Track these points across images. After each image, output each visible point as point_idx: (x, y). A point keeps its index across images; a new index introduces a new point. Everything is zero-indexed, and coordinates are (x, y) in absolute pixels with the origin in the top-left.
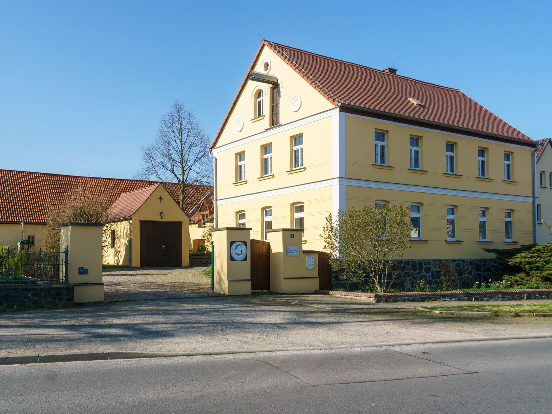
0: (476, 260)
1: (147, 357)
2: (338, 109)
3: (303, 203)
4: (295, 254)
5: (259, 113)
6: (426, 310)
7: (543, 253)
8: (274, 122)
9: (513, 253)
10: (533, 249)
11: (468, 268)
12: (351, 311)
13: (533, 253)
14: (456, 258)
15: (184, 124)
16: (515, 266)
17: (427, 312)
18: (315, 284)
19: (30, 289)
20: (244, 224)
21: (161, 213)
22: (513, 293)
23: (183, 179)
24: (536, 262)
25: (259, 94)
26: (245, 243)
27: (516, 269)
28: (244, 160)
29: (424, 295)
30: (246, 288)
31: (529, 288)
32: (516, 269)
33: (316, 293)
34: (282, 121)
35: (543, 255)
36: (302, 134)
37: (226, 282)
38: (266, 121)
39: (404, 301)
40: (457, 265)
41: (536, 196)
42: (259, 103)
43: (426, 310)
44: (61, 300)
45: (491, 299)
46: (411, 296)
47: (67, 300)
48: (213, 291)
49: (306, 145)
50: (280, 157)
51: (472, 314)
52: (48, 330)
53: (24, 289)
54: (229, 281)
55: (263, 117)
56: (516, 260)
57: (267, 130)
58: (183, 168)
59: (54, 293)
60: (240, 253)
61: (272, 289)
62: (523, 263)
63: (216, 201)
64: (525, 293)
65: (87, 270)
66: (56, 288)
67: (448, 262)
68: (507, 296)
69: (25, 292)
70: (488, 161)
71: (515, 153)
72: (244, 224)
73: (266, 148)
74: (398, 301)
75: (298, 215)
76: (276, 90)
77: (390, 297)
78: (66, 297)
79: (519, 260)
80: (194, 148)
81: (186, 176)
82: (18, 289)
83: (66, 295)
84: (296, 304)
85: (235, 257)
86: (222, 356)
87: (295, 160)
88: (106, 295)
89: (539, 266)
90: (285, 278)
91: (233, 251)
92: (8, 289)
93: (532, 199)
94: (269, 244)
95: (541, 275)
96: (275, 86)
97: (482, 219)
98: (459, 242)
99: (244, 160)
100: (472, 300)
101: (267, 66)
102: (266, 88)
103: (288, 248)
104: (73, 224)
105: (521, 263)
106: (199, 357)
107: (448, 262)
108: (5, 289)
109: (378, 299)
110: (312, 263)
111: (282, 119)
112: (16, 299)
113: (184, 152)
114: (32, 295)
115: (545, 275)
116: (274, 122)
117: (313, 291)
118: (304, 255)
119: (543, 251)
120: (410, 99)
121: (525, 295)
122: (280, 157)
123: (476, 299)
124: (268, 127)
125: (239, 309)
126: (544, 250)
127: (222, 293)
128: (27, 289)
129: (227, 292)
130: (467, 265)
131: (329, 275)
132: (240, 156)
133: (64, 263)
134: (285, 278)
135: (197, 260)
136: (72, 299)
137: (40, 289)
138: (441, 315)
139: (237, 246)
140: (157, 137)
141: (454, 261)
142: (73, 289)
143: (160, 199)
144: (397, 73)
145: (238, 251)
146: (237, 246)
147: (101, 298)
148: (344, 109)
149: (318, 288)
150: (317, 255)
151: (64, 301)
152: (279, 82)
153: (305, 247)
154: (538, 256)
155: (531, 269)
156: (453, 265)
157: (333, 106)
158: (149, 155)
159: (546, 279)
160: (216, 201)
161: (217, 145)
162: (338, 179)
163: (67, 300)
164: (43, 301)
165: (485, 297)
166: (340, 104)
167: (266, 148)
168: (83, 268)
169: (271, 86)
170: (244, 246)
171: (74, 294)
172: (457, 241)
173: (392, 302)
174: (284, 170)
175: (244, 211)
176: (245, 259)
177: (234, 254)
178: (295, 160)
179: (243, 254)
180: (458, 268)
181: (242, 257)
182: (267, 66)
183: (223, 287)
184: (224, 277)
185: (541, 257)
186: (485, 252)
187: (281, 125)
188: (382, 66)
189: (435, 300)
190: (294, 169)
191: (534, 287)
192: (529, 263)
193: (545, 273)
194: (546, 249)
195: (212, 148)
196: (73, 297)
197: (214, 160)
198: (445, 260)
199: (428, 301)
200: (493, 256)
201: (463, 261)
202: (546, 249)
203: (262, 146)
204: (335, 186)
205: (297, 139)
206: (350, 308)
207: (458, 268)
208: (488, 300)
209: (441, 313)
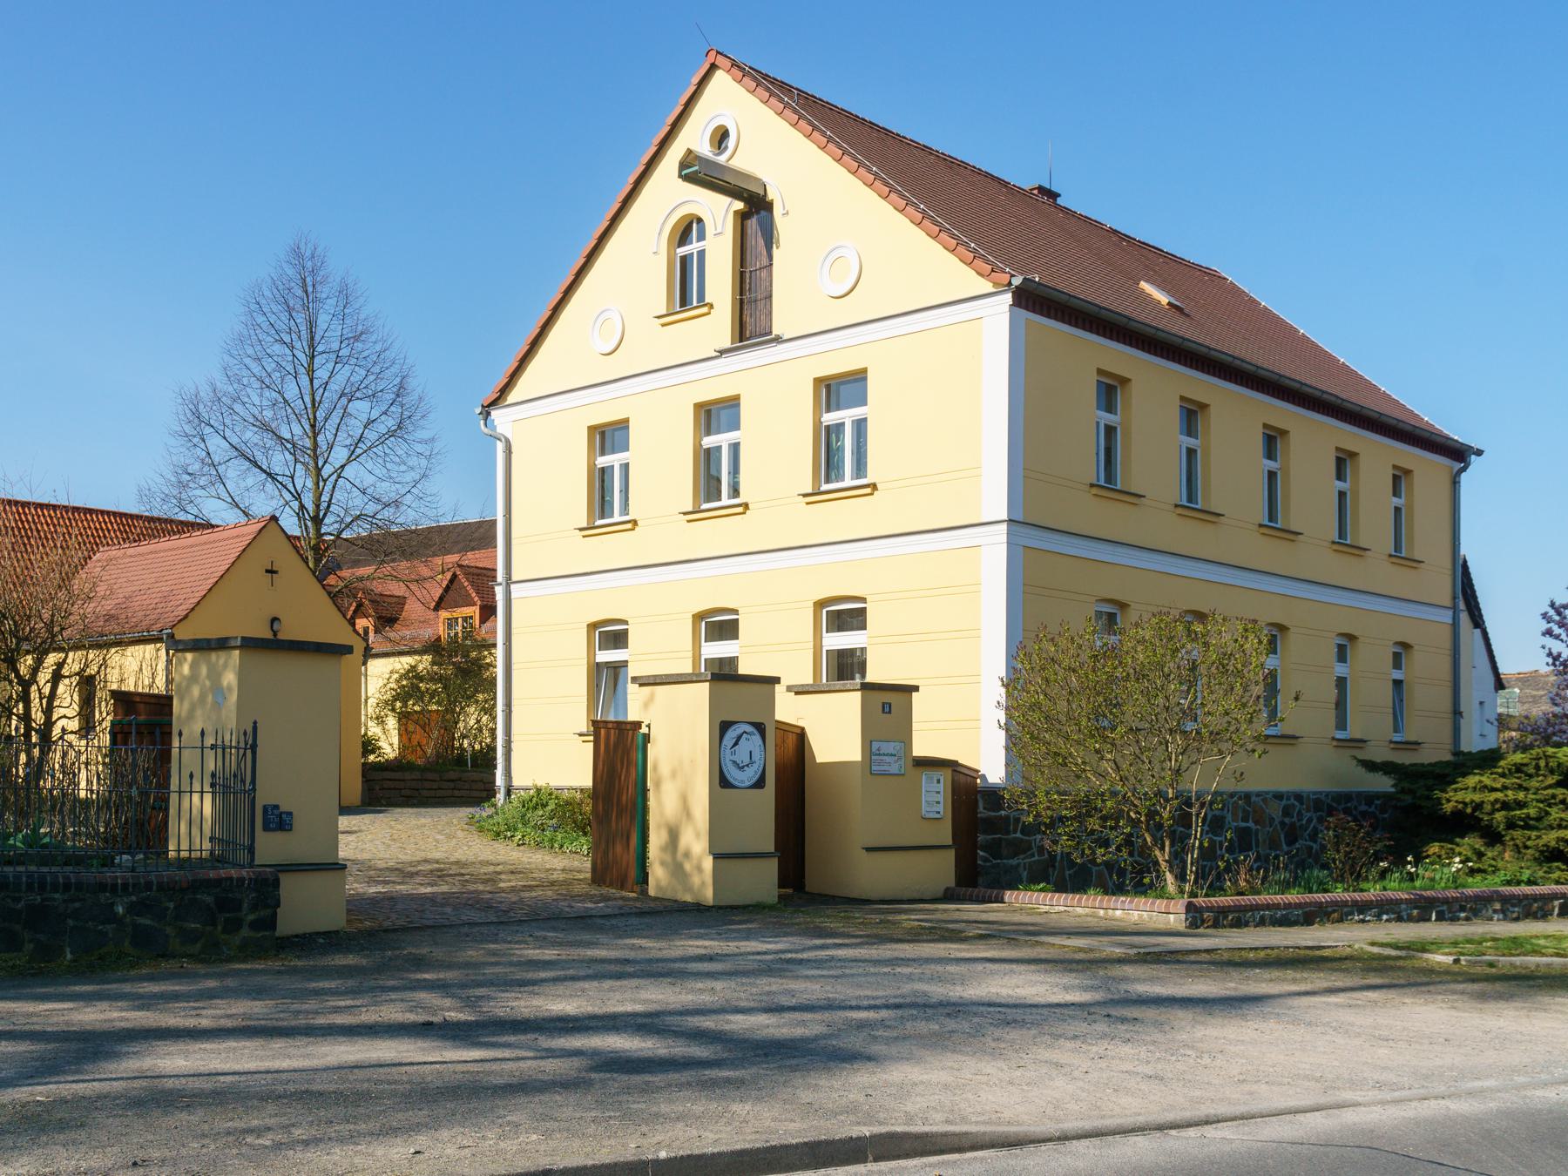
0: (1315, 793)
1: (982, 1147)
2: (1008, 298)
3: (863, 600)
4: (894, 769)
5: (685, 289)
6: (1394, 953)
7: (1531, 776)
8: (751, 324)
9: (1446, 775)
10: (1502, 763)
11: (1310, 820)
12: (1192, 957)
13: (1503, 775)
14: (1283, 788)
15: (323, 320)
16: (1458, 814)
17: (1399, 958)
18: (941, 868)
19: (125, 886)
20: (733, 661)
21: (274, 620)
22: (1526, 896)
23: (318, 506)
24: (1521, 805)
25: (688, 229)
26: (760, 728)
27: (1462, 823)
28: (626, 449)
29: (1310, 904)
30: (763, 880)
31: (1509, 883)
32: (1462, 823)
33: (949, 896)
34: (781, 324)
35: (1534, 783)
36: (864, 371)
37: (708, 863)
38: (718, 324)
39: (1262, 923)
40: (1287, 812)
41: (265, 633)
42: (685, 261)
43: (1394, 953)
44: (234, 926)
45: (1476, 915)
46: (1277, 906)
47: (254, 926)
48: (645, 892)
49: (878, 409)
50: (776, 443)
51: (1549, 965)
52: (204, 1043)
53: (102, 887)
54: (717, 857)
55: (705, 310)
56: (1460, 796)
57: (722, 352)
58: (319, 470)
59: (209, 899)
60: (747, 761)
61: (812, 883)
62: (1488, 807)
63: (508, 585)
64: (1555, 896)
65: (290, 814)
66: (218, 882)
67: (1265, 800)
68: (1514, 905)
69: (104, 897)
70: (1356, 493)
71: (1416, 474)
72: (733, 661)
73: (716, 414)
74: (1247, 925)
75: (839, 641)
76: (753, 223)
77: (1222, 912)
78: (251, 917)
79: (1469, 797)
80: (355, 406)
81: (325, 498)
82: (79, 886)
83: (254, 908)
84: (981, 937)
85: (733, 774)
86: (1210, 1131)
87: (835, 459)
88: (358, 906)
89: (1528, 816)
90: (868, 849)
91: (727, 757)
92: (42, 886)
93: (1450, 613)
94: (801, 735)
95: (1541, 842)
96: (756, 207)
97: (1341, 670)
98: (1290, 739)
99: (626, 449)
100: (1429, 920)
101: (720, 137)
102: (719, 211)
103: (875, 745)
104: (250, 644)
105: (1478, 806)
106: (1139, 1141)
107: (1265, 800)
108: (30, 887)
109: (1196, 917)
110: (935, 796)
111: (784, 316)
112: (71, 922)
113: (320, 414)
114: (131, 909)
115: (1553, 844)
116: (751, 324)
117: (940, 894)
118: (919, 769)
119: (1532, 771)
120: (1144, 285)
121: (1556, 903)
122: (776, 443)
123: (1506, 916)
124: (728, 344)
125: (840, 953)
126: (1537, 767)
127: (688, 898)
128: (114, 886)
129: (708, 896)
130: (1308, 810)
131: (991, 842)
132: (609, 436)
133: (207, 788)
134: (868, 849)
135: (387, 784)
136: (271, 923)
137: (161, 887)
138: (1456, 968)
139: (739, 738)
140: (227, 358)
141: (1279, 796)
142: (276, 883)
143: (271, 572)
144: (1059, 201)
145: (742, 754)
146: (739, 738)
147: (335, 919)
148: (1029, 299)
149: (951, 882)
150: (945, 776)
151: (245, 932)
152: (770, 196)
153: (920, 749)
154: (1520, 787)
155: (1511, 825)
156: (1275, 810)
157: (988, 287)
158: (197, 419)
159: (1552, 856)
160: (508, 585)
161: (512, 397)
162: (1004, 527)
163: (254, 926)
164: (169, 930)
165: (1463, 909)
166: (1017, 281)
167: (709, 412)
168: (276, 807)
169: (739, 205)
170: (757, 738)
171: (278, 905)
172: (1283, 736)
173: (1232, 926)
174: (760, 486)
175: (626, 622)
176: (760, 783)
177: (730, 765)
178: (835, 459)
179: (755, 766)
180: (1287, 820)
181: (750, 776)
182: (720, 137)
183: (696, 880)
184: (696, 842)
185: (1526, 789)
186: (1361, 771)
187: (778, 340)
188: (1025, 178)
189: (1340, 920)
190: (825, 487)
191: (1525, 878)
192: (1505, 806)
193: (1550, 838)
194: (1542, 763)
195: (494, 403)
196: (275, 915)
197: (500, 446)
198: (1258, 795)
199: (1322, 923)
200: (1383, 784)
201: (1298, 797)
202: (1542, 763)
203: (698, 407)
204: (993, 551)
205: (839, 389)
206: (1185, 947)
207: (1287, 820)
208: (1467, 919)
209: (1457, 961)
